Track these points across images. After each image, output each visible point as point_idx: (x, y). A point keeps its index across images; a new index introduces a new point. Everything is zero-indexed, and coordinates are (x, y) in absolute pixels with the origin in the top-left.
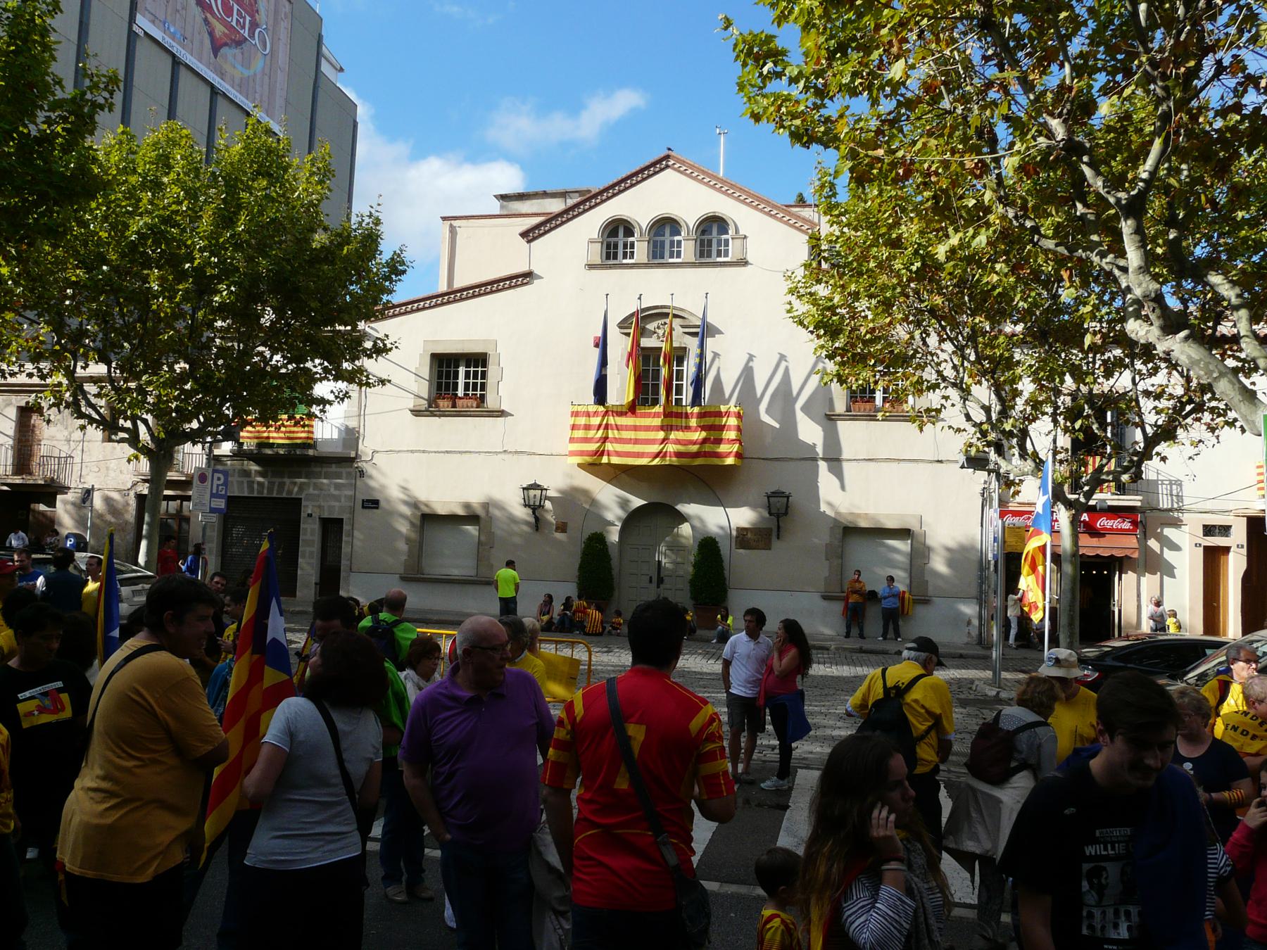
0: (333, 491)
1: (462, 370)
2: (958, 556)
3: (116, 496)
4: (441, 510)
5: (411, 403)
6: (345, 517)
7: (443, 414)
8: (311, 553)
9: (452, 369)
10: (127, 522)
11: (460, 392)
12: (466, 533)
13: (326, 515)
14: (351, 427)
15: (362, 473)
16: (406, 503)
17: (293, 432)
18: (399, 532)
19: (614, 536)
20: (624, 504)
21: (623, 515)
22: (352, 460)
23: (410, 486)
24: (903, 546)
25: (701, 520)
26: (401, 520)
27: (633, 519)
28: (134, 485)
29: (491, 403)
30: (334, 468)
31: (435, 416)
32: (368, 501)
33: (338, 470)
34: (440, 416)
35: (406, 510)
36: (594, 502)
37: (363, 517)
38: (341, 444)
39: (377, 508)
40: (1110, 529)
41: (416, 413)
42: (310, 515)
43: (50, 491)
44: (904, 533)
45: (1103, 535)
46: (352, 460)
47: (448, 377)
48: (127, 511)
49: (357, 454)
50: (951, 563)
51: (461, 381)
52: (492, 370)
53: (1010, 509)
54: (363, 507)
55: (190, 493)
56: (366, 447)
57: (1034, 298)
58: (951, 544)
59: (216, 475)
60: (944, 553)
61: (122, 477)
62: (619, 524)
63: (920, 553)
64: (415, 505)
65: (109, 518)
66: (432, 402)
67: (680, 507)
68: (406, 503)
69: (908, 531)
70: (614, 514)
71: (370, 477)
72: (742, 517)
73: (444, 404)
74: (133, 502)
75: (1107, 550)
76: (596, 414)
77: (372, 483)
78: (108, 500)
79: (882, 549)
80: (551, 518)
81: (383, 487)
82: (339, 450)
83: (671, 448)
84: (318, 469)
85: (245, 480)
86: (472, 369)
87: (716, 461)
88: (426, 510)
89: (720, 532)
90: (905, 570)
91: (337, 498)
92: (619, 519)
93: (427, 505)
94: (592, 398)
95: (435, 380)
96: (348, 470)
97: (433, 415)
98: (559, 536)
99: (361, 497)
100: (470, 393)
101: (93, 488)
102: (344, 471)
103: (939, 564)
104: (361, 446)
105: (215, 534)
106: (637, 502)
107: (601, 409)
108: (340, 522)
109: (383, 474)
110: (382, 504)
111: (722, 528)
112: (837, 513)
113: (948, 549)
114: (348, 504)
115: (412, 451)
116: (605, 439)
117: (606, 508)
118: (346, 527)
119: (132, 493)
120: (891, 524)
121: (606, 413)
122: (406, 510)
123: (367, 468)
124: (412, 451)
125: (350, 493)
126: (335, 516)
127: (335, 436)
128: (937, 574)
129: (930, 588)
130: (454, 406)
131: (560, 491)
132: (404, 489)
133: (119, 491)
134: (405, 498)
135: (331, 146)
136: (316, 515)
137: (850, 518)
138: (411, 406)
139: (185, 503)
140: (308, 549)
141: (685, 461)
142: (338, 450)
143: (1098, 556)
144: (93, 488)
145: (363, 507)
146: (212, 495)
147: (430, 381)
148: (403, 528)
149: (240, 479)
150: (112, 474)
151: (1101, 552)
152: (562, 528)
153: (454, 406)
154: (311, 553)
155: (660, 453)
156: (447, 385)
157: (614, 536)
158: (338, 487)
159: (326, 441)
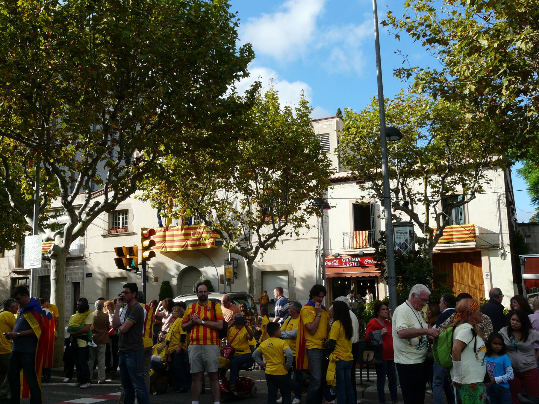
0: (76, 271)
2: (306, 280)
5: (102, 232)
6: (80, 281)
7: (113, 236)
8: (69, 297)
9: (117, 217)
10: (7, 290)
11: (121, 226)
13: (74, 281)
14: (82, 244)
15: (86, 263)
16: (100, 274)
17: (449, 235)
18: (98, 286)
20: (178, 268)
21: (178, 272)
22: (82, 258)
24: (285, 278)
25: (206, 272)
26: (99, 281)
27: (183, 275)
28: (10, 274)
29: (130, 230)
30: (76, 262)
31: (110, 237)
32: (88, 274)
33: (78, 262)
34: (112, 237)
35: (99, 277)
36: (166, 268)
37: (87, 280)
38: (78, 251)
39: (91, 277)
40: (370, 264)
41: (104, 236)
42: (68, 282)
43: (430, 298)
44: (285, 272)
45: (368, 267)
46: (82, 258)
47: (116, 220)
48: (7, 285)
49: (84, 255)
50: (303, 285)
51: (121, 221)
52: (130, 216)
53: (329, 258)
54: (87, 277)
56: (87, 253)
58: (303, 276)
60: (301, 281)
61: (6, 271)
62: (177, 277)
63: (292, 281)
64: (102, 274)
66: (109, 231)
68: (100, 274)
69: (287, 271)
70: (174, 272)
71: (88, 264)
72: (221, 270)
73: (113, 232)
74: (9, 281)
75: (368, 274)
76: (161, 231)
77: (88, 266)
79: (278, 281)
80: (152, 276)
81: (92, 268)
82: (78, 254)
84: (71, 262)
85: (46, 269)
86: (124, 216)
87: (202, 247)
88: (107, 276)
92: (176, 274)
93: (107, 274)
94: (158, 225)
95: (112, 222)
96: (81, 262)
98: (155, 283)
99: (86, 273)
100: (124, 226)
102: (80, 262)
103: (299, 286)
104: (85, 252)
106: (183, 267)
109: (91, 262)
110: (93, 275)
111: (214, 275)
112: (258, 266)
113: (302, 279)
114: (81, 276)
115: (103, 252)
116: (165, 241)
117: (170, 270)
118: (81, 286)
119: (9, 277)
120: (278, 269)
122: (99, 277)
123: (88, 262)
124: (103, 252)
126: (77, 281)
127: (77, 248)
128: (298, 290)
129: (297, 296)
130: (117, 232)
131: (154, 264)
132: (99, 268)
133: (4, 277)
134: (99, 272)
136: (70, 281)
137: (263, 268)
138: (102, 234)
139: (28, 280)
141: (196, 248)
142: (77, 254)
143: (364, 277)
145: (87, 277)
148: (100, 284)
149: (45, 269)
151: (364, 275)
152: (156, 280)
153: (117, 232)
154: (69, 297)
155: (184, 245)
156: (116, 223)
158: (78, 269)
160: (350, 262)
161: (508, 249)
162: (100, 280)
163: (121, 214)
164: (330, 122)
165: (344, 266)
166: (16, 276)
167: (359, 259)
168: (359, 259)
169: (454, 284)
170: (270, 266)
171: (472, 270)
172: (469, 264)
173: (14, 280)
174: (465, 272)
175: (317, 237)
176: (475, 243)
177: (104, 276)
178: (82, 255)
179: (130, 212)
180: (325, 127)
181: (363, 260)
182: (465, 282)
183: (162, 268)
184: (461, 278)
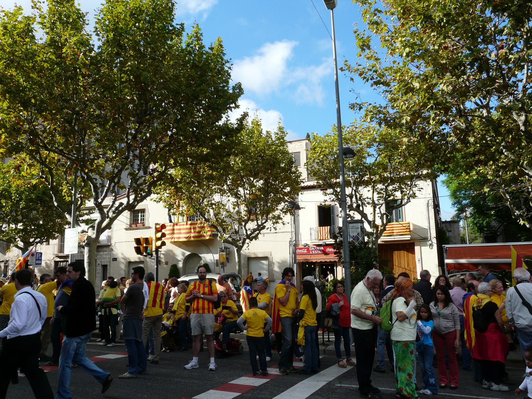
0: (104, 256)
1: (140, 214)
3: (48, 262)
4: (132, 260)
6: (108, 264)
10: (51, 270)
11: (139, 222)
12: (263, 264)
15: (112, 250)
16: (123, 258)
19: (180, 265)
20: (183, 254)
21: (183, 258)
22: (109, 246)
23: (124, 253)
28: (54, 258)
29: (146, 225)
30: (105, 249)
35: (123, 261)
36: (174, 254)
41: (126, 229)
42: (99, 264)
44: (266, 258)
45: (329, 254)
46: (109, 246)
50: (279, 267)
51: (140, 218)
52: (146, 214)
55: (68, 260)
57: (222, 160)
58: (279, 261)
59: (38, 254)
60: (278, 264)
63: (271, 264)
64: (125, 259)
65: (47, 269)
66: (130, 226)
67: (200, 255)
71: (114, 251)
73: (134, 226)
74: (53, 264)
76: (170, 226)
78: (46, 263)
79: (260, 264)
80: (163, 260)
81: (117, 254)
82: (106, 243)
83: (192, 235)
85: (82, 254)
87: (203, 238)
88: (128, 260)
89: (210, 261)
90: (266, 270)
91: (105, 258)
92: (182, 259)
97: (130, 230)
99: (112, 258)
101: (9, 260)
102: (107, 249)
103: (276, 269)
104: (112, 242)
105: (100, 271)
106: (187, 253)
107: (172, 224)
108: (107, 265)
109: (117, 249)
110: (118, 259)
111: (211, 260)
113: (279, 263)
115: (125, 242)
116: (173, 233)
117: (177, 256)
118: (108, 267)
119: (53, 261)
120: (260, 255)
121: (173, 226)
122: (123, 261)
124: (125, 242)
125: (109, 256)
127: (105, 239)
128: (276, 272)
130: (136, 226)
131: (165, 252)
133: (49, 260)
134: (123, 257)
135: (75, 129)
136: (100, 264)
138: (125, 228)
140: (98, 275)
142: (105, 243)
144: (9, 260)
146: (36, 260)
147: (130, 219)
148: (123, 267)
150: (48, 255)
151: (326, 260)
152: (167, 263)
153: (136, 226)
156: (136, 219)
157: (180, 265)
159: (103, 240)
160: (315, 250)
161: (434, 241)
162: (123, 263)
163: (140, 212)
164: (301, 144)
165: (311, 253)
166: (58, 260)
167: (322, 248)
168: (322, 248)
169: (394, 267)
170: (254, 254)
171: (408, 256)
172: (405, 252)
173: (56, 263)
174: (402, 258)
175: (290, 231)
176: (410, 236)
177: (127, 260)
178: (109, 244)
179: (146, 211)
180: (297, 147)
181: (325, 249)
182: (403, 266)
183: (171, 254)
184: (400, 263)
